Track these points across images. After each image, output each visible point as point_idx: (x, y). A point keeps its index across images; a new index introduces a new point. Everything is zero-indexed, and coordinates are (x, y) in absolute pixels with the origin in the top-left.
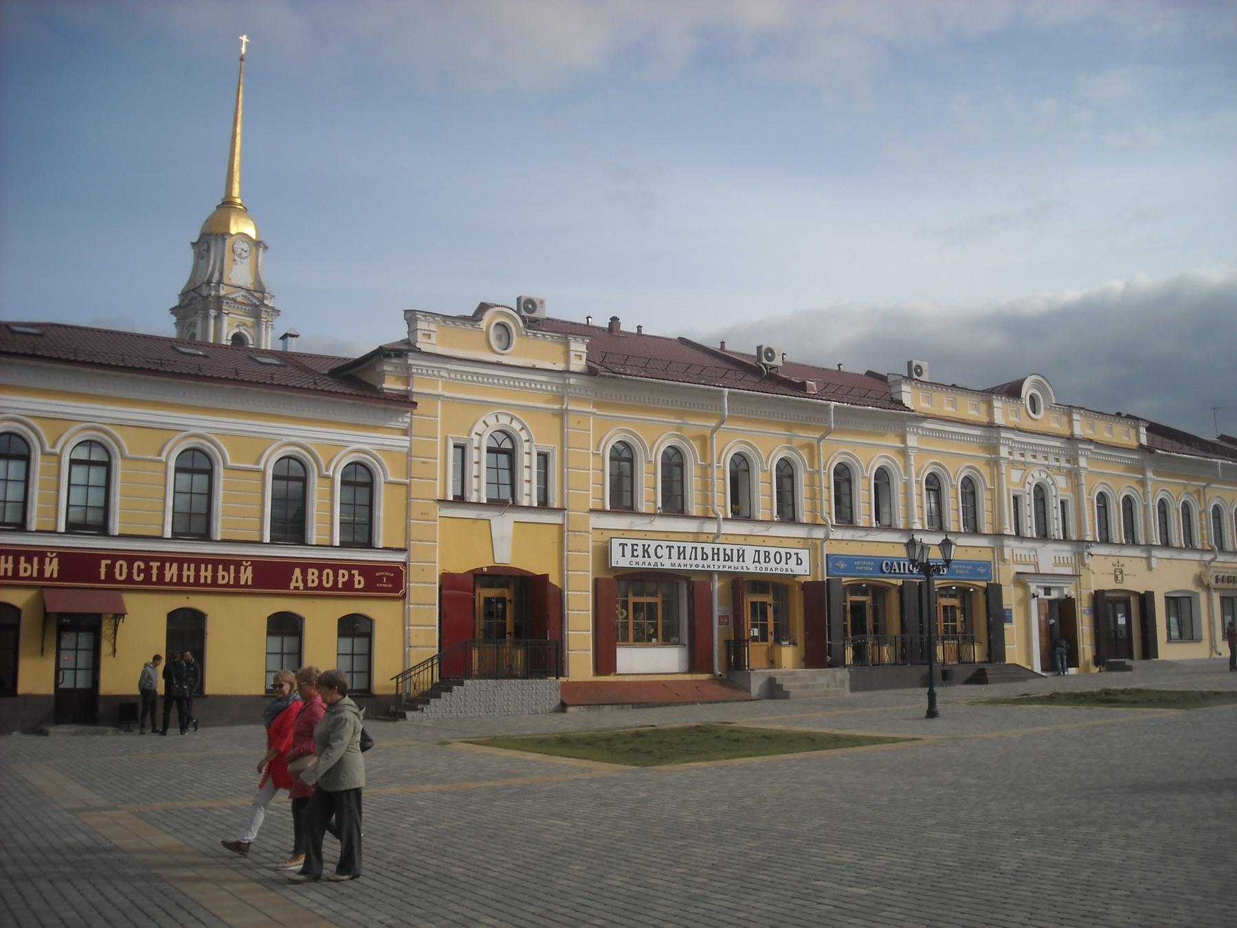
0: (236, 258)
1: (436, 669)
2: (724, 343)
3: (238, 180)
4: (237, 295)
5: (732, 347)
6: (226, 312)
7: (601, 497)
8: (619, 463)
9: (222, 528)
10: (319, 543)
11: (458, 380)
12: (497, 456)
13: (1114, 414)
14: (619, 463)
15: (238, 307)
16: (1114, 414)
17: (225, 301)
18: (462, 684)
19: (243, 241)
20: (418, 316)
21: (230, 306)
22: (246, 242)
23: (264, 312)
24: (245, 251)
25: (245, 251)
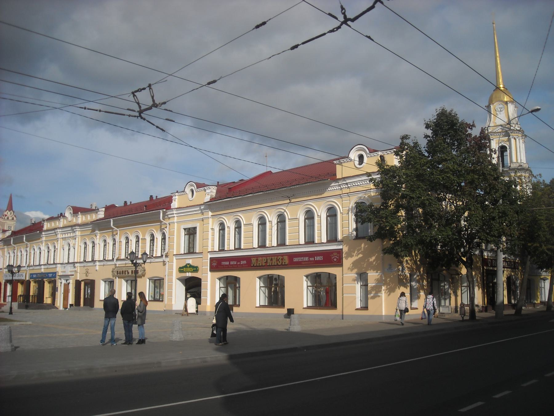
0: (497, 113)
1: (36, 298)
2: (62, 213)
3: (499, 69)
4: (497, 129)
5: (385, 158)
6: (492, 139)
7: (359, 236)
8: (13, 278)
9: (317, 224)
10: (177, 254)
11: (361, 185)
12: (8, 312)
13: (328, 13)
14: (13, 278)
15: (516, 132)
16: (328, 13)
17: (490, 134)
18: (394, 256)
19: (500, 104)
20: (341, 161)
21: (515, 133)
22: (501, 104)
23: (511, 133)
24: (501, 108)
25: (501, 108)
